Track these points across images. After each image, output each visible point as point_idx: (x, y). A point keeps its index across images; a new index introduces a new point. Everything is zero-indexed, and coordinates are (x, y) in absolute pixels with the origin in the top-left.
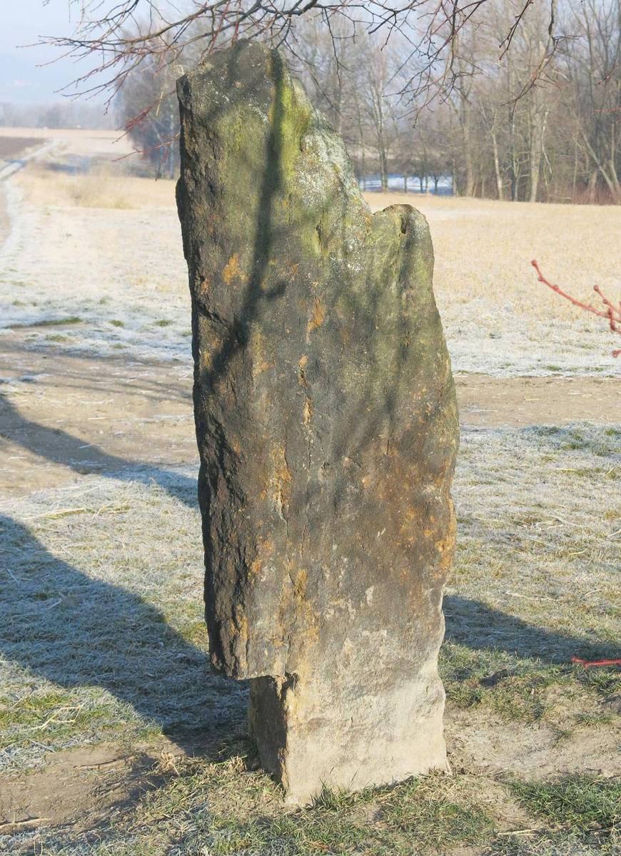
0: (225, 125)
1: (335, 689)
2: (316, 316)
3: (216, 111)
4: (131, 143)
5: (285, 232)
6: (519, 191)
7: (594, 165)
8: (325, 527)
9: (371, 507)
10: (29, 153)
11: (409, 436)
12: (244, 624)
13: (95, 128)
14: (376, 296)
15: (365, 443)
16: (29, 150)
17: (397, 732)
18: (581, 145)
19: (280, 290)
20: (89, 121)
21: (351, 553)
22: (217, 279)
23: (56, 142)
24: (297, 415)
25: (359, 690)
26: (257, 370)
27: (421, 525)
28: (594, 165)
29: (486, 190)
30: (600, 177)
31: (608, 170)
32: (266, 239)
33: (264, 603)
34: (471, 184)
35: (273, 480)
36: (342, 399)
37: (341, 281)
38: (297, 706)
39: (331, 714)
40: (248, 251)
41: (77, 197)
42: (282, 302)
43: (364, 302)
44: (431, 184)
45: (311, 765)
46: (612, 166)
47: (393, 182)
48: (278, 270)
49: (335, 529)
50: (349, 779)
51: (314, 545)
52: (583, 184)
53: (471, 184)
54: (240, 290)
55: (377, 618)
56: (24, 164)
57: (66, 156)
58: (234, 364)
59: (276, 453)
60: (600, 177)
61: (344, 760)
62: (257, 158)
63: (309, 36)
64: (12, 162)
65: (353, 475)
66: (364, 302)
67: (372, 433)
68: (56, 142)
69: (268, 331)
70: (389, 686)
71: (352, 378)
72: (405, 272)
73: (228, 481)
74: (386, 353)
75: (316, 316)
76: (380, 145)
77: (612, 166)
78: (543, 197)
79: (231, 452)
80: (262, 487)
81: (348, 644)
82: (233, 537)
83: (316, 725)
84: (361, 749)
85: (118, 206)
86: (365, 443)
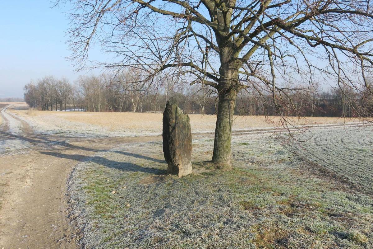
0: (173, 106)
1: (183, 165)
2: (181, 126)
3: (172, 105)
4: (27, 104)
5: (178, 117)
6: (97, 111)
7: (108, 106)
8: (181, 148)
9: (185, 146)
10: (7, 107)
11: (189, 138)
12: (175, 158)
13: (17, 102)
14: (185, 123)
15: (185, 139)
16: (6, 106)
17: (188, 169)
18: (106, 103)
19: (178, 123)
20: (18, 100)
21: (183, 150)
22: (172, 122)
23: (11, 104)
24: (179, 136)
25: (185, 165)
26: (177, 131)
27: (190, 147)
28: (108, 106)
29: (92, 110)
30: (109, 108)
31: (110, 106)
32: (176, 118)
33: (177, 156)
34: (89, 110)
35: (177, 143)
36: (184, 134)
37: (182, 122)
38: (180, 167)
39: (183, 168)
40: (175, 119)
41: (27, 114)
42: (178, 124)
43: (184, 124)
44: (83, 110)
45: (181, 173)
46: (111, 106)
47: (76, 110)
48: (178, 121)
49: (182, 148)
50: (185, 174)
51: (180, 150)
52: (107, 109)
53: (89, 110)
54: (174, 123)
55: (186, 157)
56: (7, 108)
57: (14, 107)
58: (174, 131)
59: (178, 140)
60: (109, 108)
61: (184, 172)
62: (175, 109)
63: (60, 86)
64: (4, 108)
65: (184, 142)
66: (184, 124)
67: (186, 137)
68: (11, 104)
69: (177, 127)
70: (188, 164)
71: (184, 132)
72: (188, 121)
73: (172, 144)
74: (187, 129)
75: (181, 126)
76: (74, 104)
77: (111, 106)
78: (101, 111)
79: (173, 140)
80: (176, 144)
81: (184, 160)
82: (173, 149)
83: (182, 169)
84: (185, 171)
85: (34, 115)
86: (185, 139)
